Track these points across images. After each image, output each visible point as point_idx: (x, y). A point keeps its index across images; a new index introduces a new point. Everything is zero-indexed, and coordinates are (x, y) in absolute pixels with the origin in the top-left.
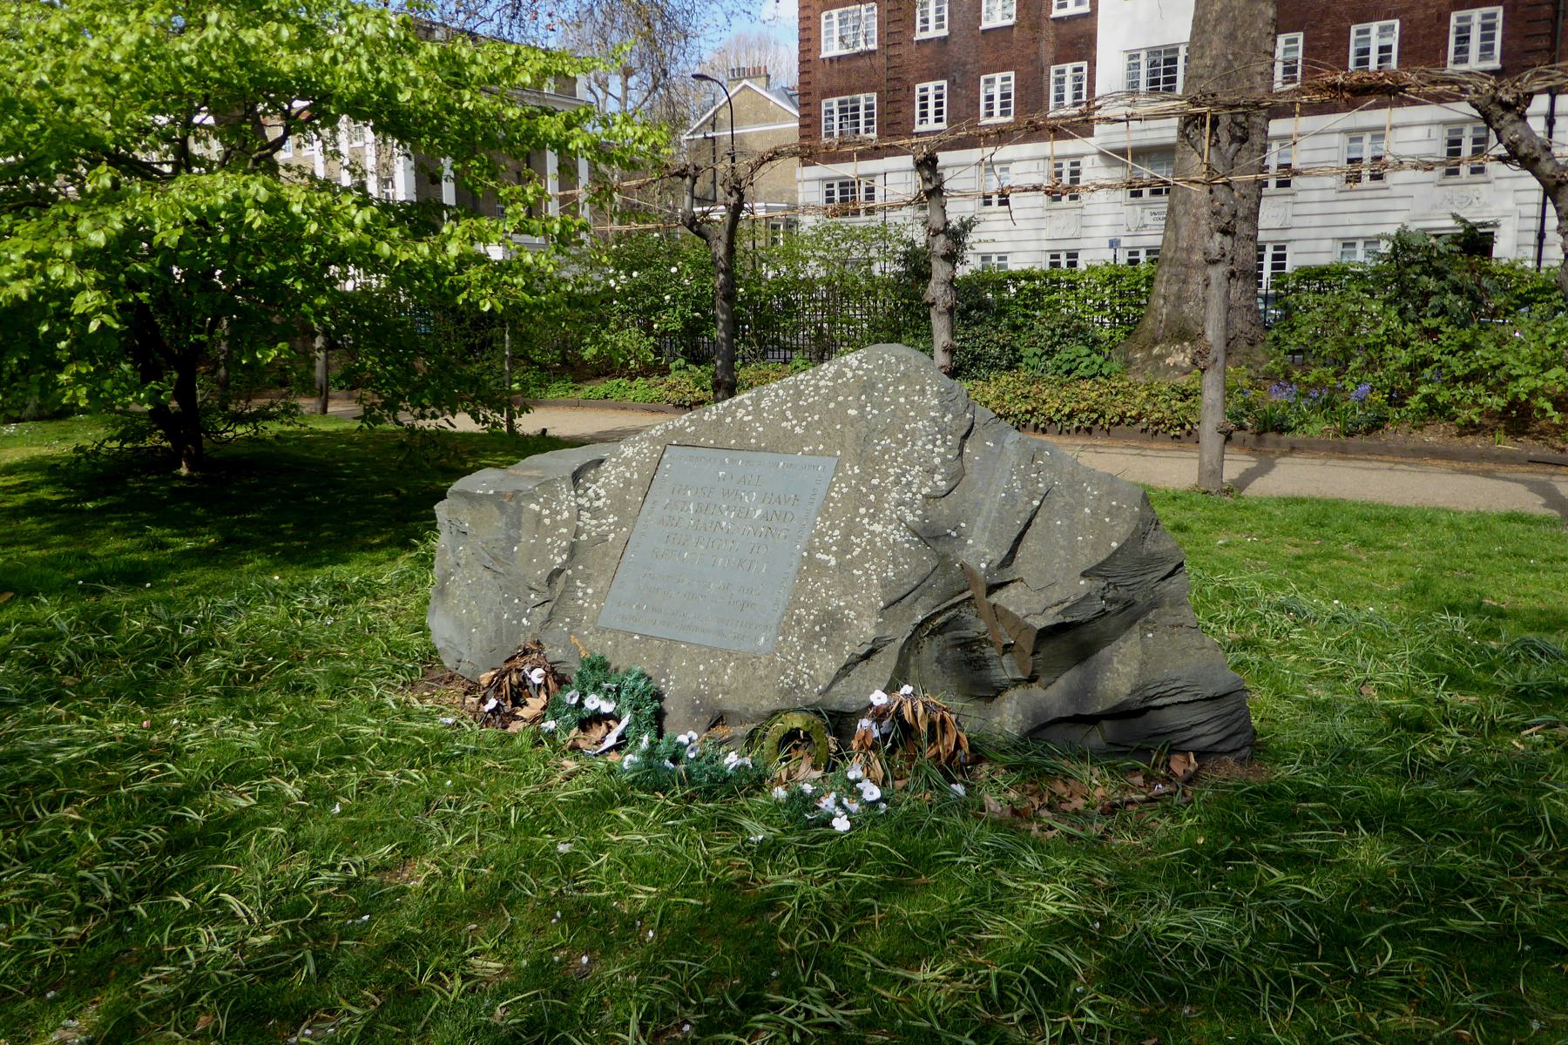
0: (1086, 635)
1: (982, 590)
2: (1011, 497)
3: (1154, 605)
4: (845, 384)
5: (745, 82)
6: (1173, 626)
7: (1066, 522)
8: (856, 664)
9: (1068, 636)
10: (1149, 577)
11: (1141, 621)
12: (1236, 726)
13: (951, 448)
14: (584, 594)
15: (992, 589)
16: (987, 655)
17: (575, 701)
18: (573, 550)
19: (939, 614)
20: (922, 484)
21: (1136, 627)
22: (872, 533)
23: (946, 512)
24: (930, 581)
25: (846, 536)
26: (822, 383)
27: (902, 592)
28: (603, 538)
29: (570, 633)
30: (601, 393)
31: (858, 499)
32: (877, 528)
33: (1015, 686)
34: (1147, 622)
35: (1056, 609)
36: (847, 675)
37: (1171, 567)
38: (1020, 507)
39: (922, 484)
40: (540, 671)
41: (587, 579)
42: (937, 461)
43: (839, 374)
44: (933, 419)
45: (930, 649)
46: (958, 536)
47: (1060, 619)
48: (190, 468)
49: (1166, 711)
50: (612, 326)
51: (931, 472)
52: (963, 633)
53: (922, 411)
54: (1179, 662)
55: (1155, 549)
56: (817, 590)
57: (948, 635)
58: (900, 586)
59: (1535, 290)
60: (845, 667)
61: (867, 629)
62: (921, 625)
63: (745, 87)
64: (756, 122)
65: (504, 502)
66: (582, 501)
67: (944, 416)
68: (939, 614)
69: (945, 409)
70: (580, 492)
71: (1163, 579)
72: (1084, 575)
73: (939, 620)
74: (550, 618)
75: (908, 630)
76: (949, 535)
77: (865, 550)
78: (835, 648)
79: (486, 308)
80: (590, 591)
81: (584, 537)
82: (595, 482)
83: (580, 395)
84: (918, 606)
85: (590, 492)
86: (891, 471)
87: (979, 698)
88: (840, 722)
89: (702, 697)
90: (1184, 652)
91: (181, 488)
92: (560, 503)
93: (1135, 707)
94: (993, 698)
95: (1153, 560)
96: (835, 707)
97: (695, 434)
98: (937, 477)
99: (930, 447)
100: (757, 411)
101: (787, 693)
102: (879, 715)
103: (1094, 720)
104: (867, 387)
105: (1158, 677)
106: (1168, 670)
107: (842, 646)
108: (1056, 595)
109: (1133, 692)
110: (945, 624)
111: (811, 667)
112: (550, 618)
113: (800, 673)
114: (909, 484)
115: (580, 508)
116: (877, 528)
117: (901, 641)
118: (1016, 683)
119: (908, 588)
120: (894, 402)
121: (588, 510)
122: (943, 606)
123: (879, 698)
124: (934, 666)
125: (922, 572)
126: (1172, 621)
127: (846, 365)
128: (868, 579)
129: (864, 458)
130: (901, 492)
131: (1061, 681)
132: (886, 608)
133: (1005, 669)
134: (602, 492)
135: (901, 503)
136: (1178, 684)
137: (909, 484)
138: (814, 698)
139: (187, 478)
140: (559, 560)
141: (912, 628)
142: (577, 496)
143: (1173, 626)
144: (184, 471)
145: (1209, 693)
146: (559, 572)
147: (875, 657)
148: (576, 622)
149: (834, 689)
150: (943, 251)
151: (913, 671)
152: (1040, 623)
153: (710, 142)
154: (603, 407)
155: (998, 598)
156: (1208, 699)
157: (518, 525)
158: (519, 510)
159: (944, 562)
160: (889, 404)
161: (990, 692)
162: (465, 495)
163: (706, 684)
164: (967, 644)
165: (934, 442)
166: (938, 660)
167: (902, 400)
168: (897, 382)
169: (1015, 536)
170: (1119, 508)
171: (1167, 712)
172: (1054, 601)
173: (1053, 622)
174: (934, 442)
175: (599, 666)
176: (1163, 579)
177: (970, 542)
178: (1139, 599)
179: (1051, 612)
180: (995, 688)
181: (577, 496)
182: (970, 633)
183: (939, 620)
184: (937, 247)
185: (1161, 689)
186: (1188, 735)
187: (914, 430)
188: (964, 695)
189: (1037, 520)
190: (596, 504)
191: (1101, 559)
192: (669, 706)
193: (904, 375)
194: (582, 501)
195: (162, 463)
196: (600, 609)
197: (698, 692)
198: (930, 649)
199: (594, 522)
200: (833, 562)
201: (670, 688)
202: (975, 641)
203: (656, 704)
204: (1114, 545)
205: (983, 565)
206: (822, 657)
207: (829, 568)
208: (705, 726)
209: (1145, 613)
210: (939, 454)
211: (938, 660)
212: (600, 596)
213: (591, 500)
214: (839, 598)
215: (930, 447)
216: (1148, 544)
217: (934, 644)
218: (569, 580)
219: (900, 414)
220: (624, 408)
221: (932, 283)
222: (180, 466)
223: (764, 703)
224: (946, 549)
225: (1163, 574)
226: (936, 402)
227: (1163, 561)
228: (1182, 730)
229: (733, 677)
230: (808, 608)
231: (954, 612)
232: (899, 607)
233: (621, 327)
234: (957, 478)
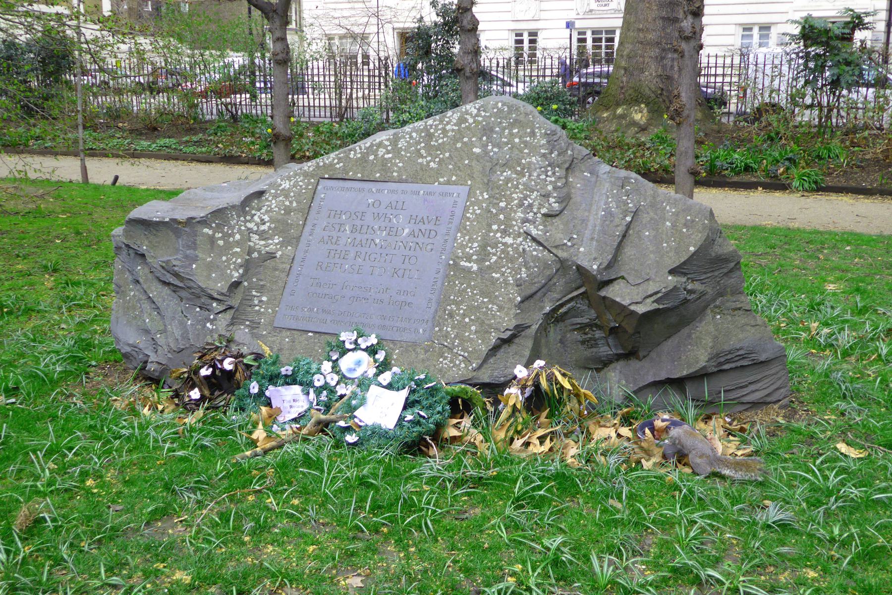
2: (609, 214)
4: (468, 128)
19: (561, 306)
22: (505, 244)
32: (509, 240)
39: (541, 206)
41: (261, 289)
43: (462, 120)
44: (544, 155)
51: (546, 196)
67: (551, 153)
68: (561, 306)
72: (672, 272)
82: (259, 209)
98: (552, 200)
105: (726, 348)
119: (538, 286)
126: (734, 305)
134: (266, 218)
137: (531, 206)
173: (649, 309)
199: (263, 242)
204: (692, 249)
215: (543, 177)
226: (544, 142)
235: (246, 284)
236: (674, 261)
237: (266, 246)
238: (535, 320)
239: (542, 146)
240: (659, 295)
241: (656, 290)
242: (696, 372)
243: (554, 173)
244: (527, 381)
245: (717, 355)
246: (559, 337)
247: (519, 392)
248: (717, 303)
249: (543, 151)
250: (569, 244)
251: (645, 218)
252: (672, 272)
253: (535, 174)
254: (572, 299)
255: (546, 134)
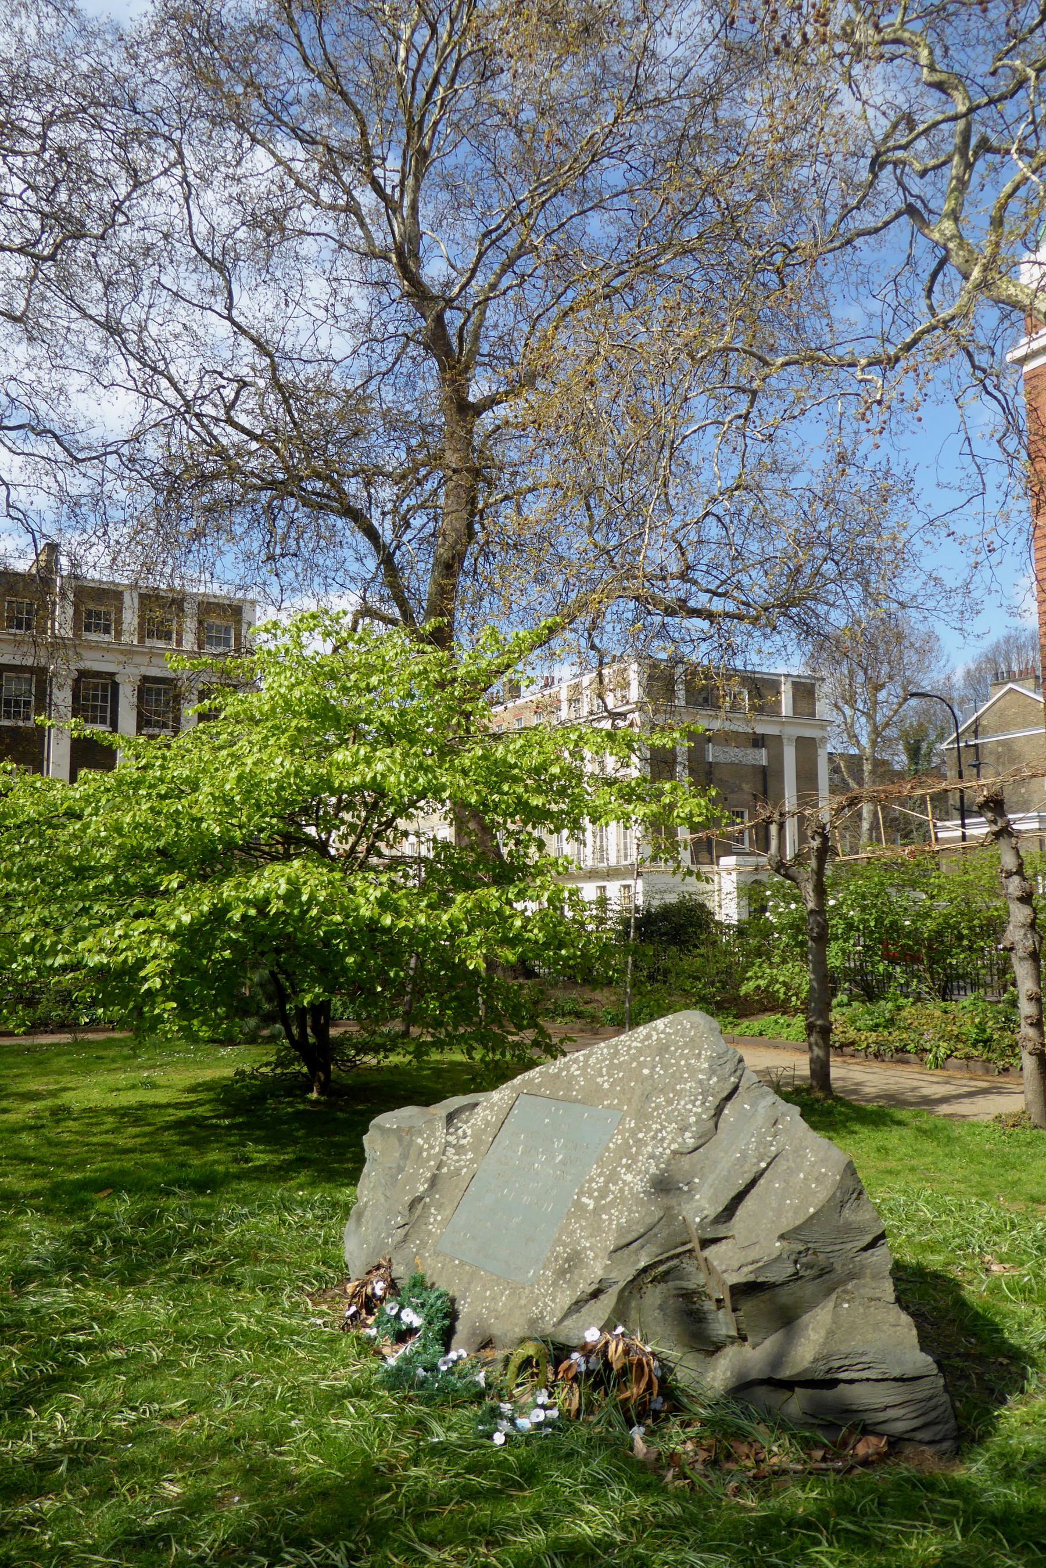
0: (784, 1296)
1: (695, 1244)
2: (744, 1156)
3: (852, 1276)
4: (649, 1046)
5: (1010, 685)
6: (871, 1299)
7: (783, 1185)
8: (587, 1301)
9: (766, 1296)
10: (849, 1246)
11: (839, 1290)
12: (933, 1415)
13: (708, 1109)
14: (435, 1217)
15: (705, 1243)
16: (706, 1308)
17: (394, 1312)
18: (434, 1181)
19: (661, 1262)
20: (673, 1141)
21: (834, 1296)
22: (624, 1182)
23: (686, 1167)
24: (656, 1230)
25: (606, 1183)
26: (634, 1044)
27: (630, 1238)
28: (458, 1170)
29: (417, 1254)
30: (756, 1030)
31: (624, 1150)
32: (629, 1178)
33: (732, 1343)
34: (845, 1292)
35: (751, 1268)
36: (578, 1311)
37: (868, 1238)
38: (746, 1168)
39: (673, 1141)
40: (381, 1285)
41: (440, 1207)
42: (693, 1119)
43: (648, 1037)
44: (700, 1081)
45: (654, 1296)
46: (690, 1191)
47: (751, 1278)
48: (320, 1093)
49: (856, 1385)
50: (776, 960)
51: (683, 1129)
52: (684, 1284)
53: (693, 1071)
54: (869, 1337)
55: (853, 1218)
56: (574, 1231)
57: (671, 1284)
58: (629, 1232)
59: (69, 1053)
60: (577, 1303)
61: (596, 1268)
62: (645, 1270)
63: (1011, 689)
64: (1025, 726)
65: (401, 1134)
66: (452, 1139)
67: (709, 1079)
68: (661, 1262)
69: (712, 1072)
70: (451, 1130)
71: (865, 1249)
72: (782, 1237)
73: (662, 1268)
74: (405, 1239)
75: (630, 1273)
76: (680, 1189)
77: (616, 1197)
78: (573, 1285)
79: (471, 967)
80: (439, 1218)
81: (445, 1170)
82: (466, 1122)
83: (737, 1031)
84: (643, 1253)
85: (460, 1132)
86: (654, 1126)
87: (698, 1350)
88: (559, 1352)
89: (481, 1320)
90: (877, 1326)
91: (305, 1111)
92: (436, 1139)
93: (819, 1376)
94: (712, 1353)
95: (850, 1230)
96: (561, 1339)
97: (540, 1085)
98: (688, 1135)
99: (690, 1106)
100: (584, 1069)
101: (533, 1322)
102: (587, 1350)
103: (789, 1385)
104: (663, 1049)
105: (844, 1348)
106: (855, 1344)
107: (577, 1283)
108: (753, 1254)
109: (816, 1360)
110: (667, 1273)
111: (553, 1301)
112: (405, 1239)
113: (546, 1305)
114: (663, 1139)
115: (448, 1144)
116: (629, 1178)
117: (622, 1284)
118: (733, 1340)
119: (635, 1235)
120: (678, 1063)
121: (454, 1146)
122: (666, 1255)
123: (592, 1335)
124: (656, 1313)
125: (649, 1221)
126: (870, 1293)
127: (655, 1029)
128: (610, 1224)
129: (642, 1116)
130: (655, 1147)
131: (767, 1343)
132: (615, 1251)
133: (723, 1324)
134: (469, 1132)
135: (652, 1156)
136: (864, 1359)
137: (663, 1139)
138: (549, 1330)
139: (316, 1102)
140: (421, 1189)
141: (635, 1273)
142: (448, 1134)
143: (871, 1299)
144: (314, 1095)
145: (896, 1373)
146: (419, 1199)
147: (602, 1297)
148: (423, 1245)
149: (566, 1323)
150: (1018, 894)
151: (634, 1315)
152: (733, 1279)
153: (972, 750)
154: (758, 1045)
155: (711, 1252)
156: (895, 1379)
157: (405, 1156)
158: (411, 1143)
159: (668, 1215)
160: (673, 1065)
161: (710, 1347)
162: (380, 1128)
163: (487, 1308)
164: (688, 1296)
165: (693, 1103)
166: (661, 1308)
167: (683, 1062)
168: (686, 1045)
169: (733, 1194)
170: (825, 1175)
171: (899, 1400)
172: (750, 1259)
173: (744, 1280)
174: (693, 1103)
175: (419, 1284)
176: (865, 1249)
177: (697, 1197)
178: (838, 1266)
179: (745, 1270)
180: (714, 1343)
181: (448, 1134)
182: (691, 1285)
183: (662, 1268)
184: (1011, 889)
185: (847, 1362)
186: (882, 1416)
187: (682, 1090)
188: (684, 1346)
189: (762, 1181)
190: (464, 1142)
191: (798, 1223)
192: (459, 1326)
193: (692, 1040)
194: (452, 1139)
195: (298, 1087)
196: (442, 1233)
197: (480, 1314)
198: (654, 1296)
199: (456, 1157)
200: (591, 1207)
201: (464, 1308)
202: (694, 1292)
203: (447, 1322)
204: (812, 1210)
205: (698, 1220)
206: (563, 1292)
207: (587, 1211)
208: (476, 1347)
209: (844, 1281)
210: (696, 1114)
211: (661, 1308)
212: (445, 1222)
213: (458, 1138)
214: (587, 1239)
215: (690, 1106)
216: (846, 1212)
217: (658, 1290)
218: (426, 1207)
219: (678, 1075)
220: (777, 1047)
221: (1011, 927)
222: (312, 1091)
223: (517, 1330)
224: (673, 1202)
225: (863, 1244)
226: (706, 1065)
227: (861, 1231)
228: (875, 1410)
229: (504, 1304)
230: (565, 1246)
231: (675, 1262)
232: (626, 1251)
233: (784, 961)
234: (704, 1139)
235: (428, 1200)
236: (789, 1221)
237: (457, 1161)
238: (623, 1275)
239: (701, 1071)
240: (760, 1264)
241: (757, 1257)
242: (799, 1374)
243: (703, 1103)
244: (595, 1347)
245: (827, 1358)
246: (659, 1302)
247: (583, 1360)
248: (849, 1286)
249: (700, 1076)
250: (686, 1188)
251: (781, 1165)
252: (782, 1237)
253: (682, 1103)
254: (677, 1256)
255: (711, 1056)
